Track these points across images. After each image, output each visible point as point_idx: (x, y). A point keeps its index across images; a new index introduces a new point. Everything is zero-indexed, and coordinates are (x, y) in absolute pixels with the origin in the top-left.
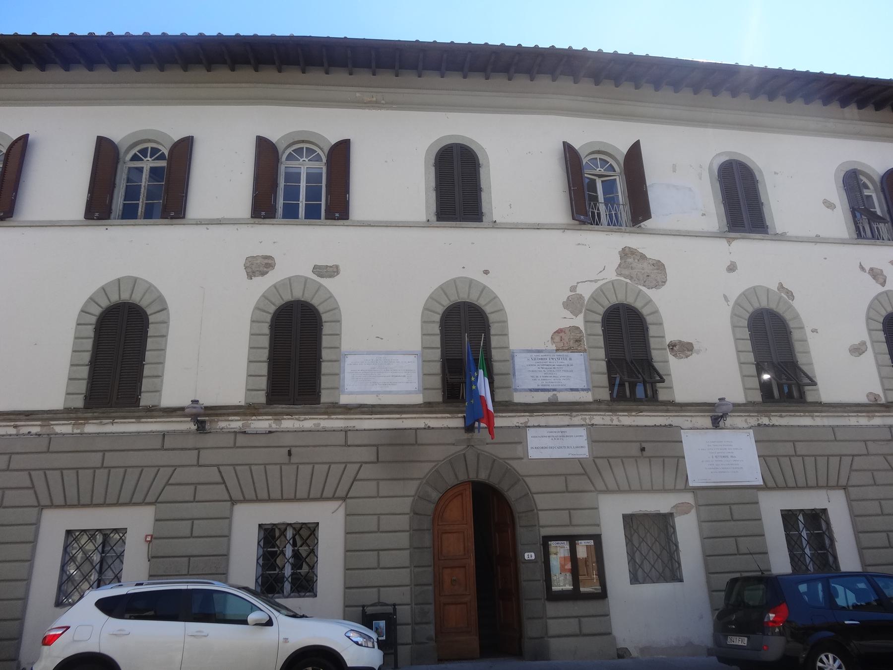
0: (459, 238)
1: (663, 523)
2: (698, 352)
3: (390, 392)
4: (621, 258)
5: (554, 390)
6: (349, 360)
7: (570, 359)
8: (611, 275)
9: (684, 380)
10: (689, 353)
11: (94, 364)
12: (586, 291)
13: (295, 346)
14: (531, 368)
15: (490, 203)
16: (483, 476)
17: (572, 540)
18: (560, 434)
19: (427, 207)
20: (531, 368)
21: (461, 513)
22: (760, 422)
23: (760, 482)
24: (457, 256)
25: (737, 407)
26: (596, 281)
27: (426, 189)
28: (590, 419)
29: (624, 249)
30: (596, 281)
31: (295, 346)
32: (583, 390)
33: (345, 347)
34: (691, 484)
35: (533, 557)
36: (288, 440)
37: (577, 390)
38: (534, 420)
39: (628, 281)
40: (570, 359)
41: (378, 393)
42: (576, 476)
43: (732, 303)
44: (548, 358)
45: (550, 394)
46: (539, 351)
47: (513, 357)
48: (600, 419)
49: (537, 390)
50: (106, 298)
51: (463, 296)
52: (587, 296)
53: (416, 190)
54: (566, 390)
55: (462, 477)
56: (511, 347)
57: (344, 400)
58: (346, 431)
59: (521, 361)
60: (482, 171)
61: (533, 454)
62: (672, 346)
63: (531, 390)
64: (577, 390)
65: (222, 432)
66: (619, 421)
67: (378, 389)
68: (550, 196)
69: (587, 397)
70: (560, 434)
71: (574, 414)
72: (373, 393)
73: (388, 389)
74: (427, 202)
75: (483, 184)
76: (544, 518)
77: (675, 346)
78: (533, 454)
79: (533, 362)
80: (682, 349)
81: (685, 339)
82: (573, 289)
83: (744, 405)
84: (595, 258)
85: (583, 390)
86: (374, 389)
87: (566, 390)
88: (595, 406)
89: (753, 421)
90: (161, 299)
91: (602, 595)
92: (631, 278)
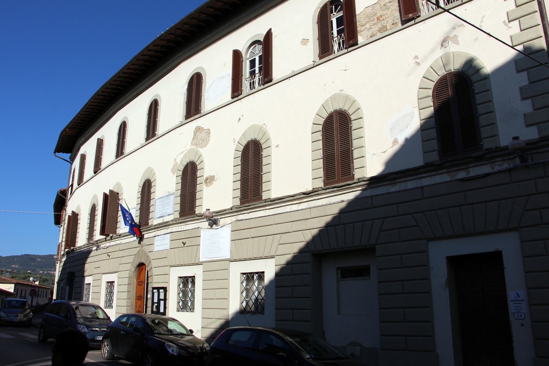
8: (189, 147)
80: (210, 180)
88: (175, 222)
89: (234, 219)
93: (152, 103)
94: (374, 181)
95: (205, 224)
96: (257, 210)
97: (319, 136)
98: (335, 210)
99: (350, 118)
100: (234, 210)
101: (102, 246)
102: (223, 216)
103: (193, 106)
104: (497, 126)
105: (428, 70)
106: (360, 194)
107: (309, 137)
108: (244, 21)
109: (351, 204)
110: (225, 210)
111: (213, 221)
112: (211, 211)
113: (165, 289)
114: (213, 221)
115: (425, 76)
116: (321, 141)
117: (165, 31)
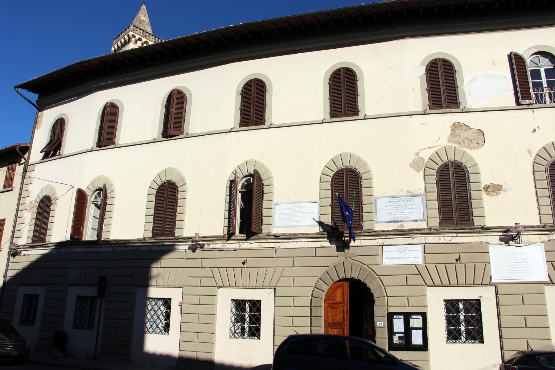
0: (346, 127)
1: (474, 306)
2: (505, 191)
3: (300, 226)
4: (452, 130)
5: (402, 221)
6: (278, 207)
7: (413, 201)
8: (444, 143)
9: (491, 211)
10: (498, 192)
11: (156, 215)
12: (426, 155)
13: (248, 202)
14: (387, 208)
15: (364, 103)
16: (355, 276)
17: (407, 316)
18: (404, 249)
19: (324, 110)
20: (387, 208)
21: (342, 296)
22: (551, 238)
23: (547, 280)
24: (346, 140)
25: (529, 229)
26: (433, 147)
27: (324, 99)
28: (425, 240)
29: (454, 124)
30: (433, 147)
31: (248, 202)
32: (421, 220)
33: (275, 200)
34: (494, 280)
35: (382, 325)
36: (245, 254)
37: (416, 221)
38: (387, 241)
39: (456, 145)
40: (413, 201)
41: (293, 227)
42: (407, 274)
43: (534, 155)
44: (398, 200)
45: (400, 224)
46: (392, 197)
47: (375, 201)
48: (430, 239)
49: (390, 222)
50: (367, 178)
51: (353, 165)
52: (426, 159)
53: (416, 93)
54: (410, 221)
55: (342, 276)
56: (374, 195)
57: (275, 231)
58: (275, 249)
59: (381, 204)
60: (359, 83)
61: (386, 262)
62: (486, 188)
63: (386, 222)
64: (416, 221)
65: (210, 250)
66: (445, 240)
67: (294, 224)
68: (504, 88)
69: (423, 225)
70: (404, 249)
71: (414, 236)
72: (291, 227)
73: (299, 224)
74: (324, 107)
75: (459, 83)
76: (391, 301)
77: (489, 187)
78: (386, 262)
79: (389, 204)
80: (494, 189)
81: (496, 183)
82: (417, 154)
83: (538, 226)
84: (435, 133)
85: (421, 220)
86: (291, 224)
87: (410, 221)
88: (430, 231)
89: (545, 238)
90: (183, 179)
91: (424, 347)
92: (459, 143)
93: (58, 120)
94: (60, 245)
95: (494, 239)
96: (367, 238)
97: (153, 198)
98: (33, 259)
99: (178, 190)
100: (547, 228)
101: (23, 253)
102: (544, 233)
103: (107, 136)
104: (275, 219)
105: (330, 161)
106: (51, 252)
107: (145, 197)
108: (398, 35)
109: (44, 256)
110: (533, 227)
111: (510, 236)
112: (200, 235)
113: (424, 315)
114: (510, 236)
115: (546, 147)
116: (154, 202)
117: (236, 24)
